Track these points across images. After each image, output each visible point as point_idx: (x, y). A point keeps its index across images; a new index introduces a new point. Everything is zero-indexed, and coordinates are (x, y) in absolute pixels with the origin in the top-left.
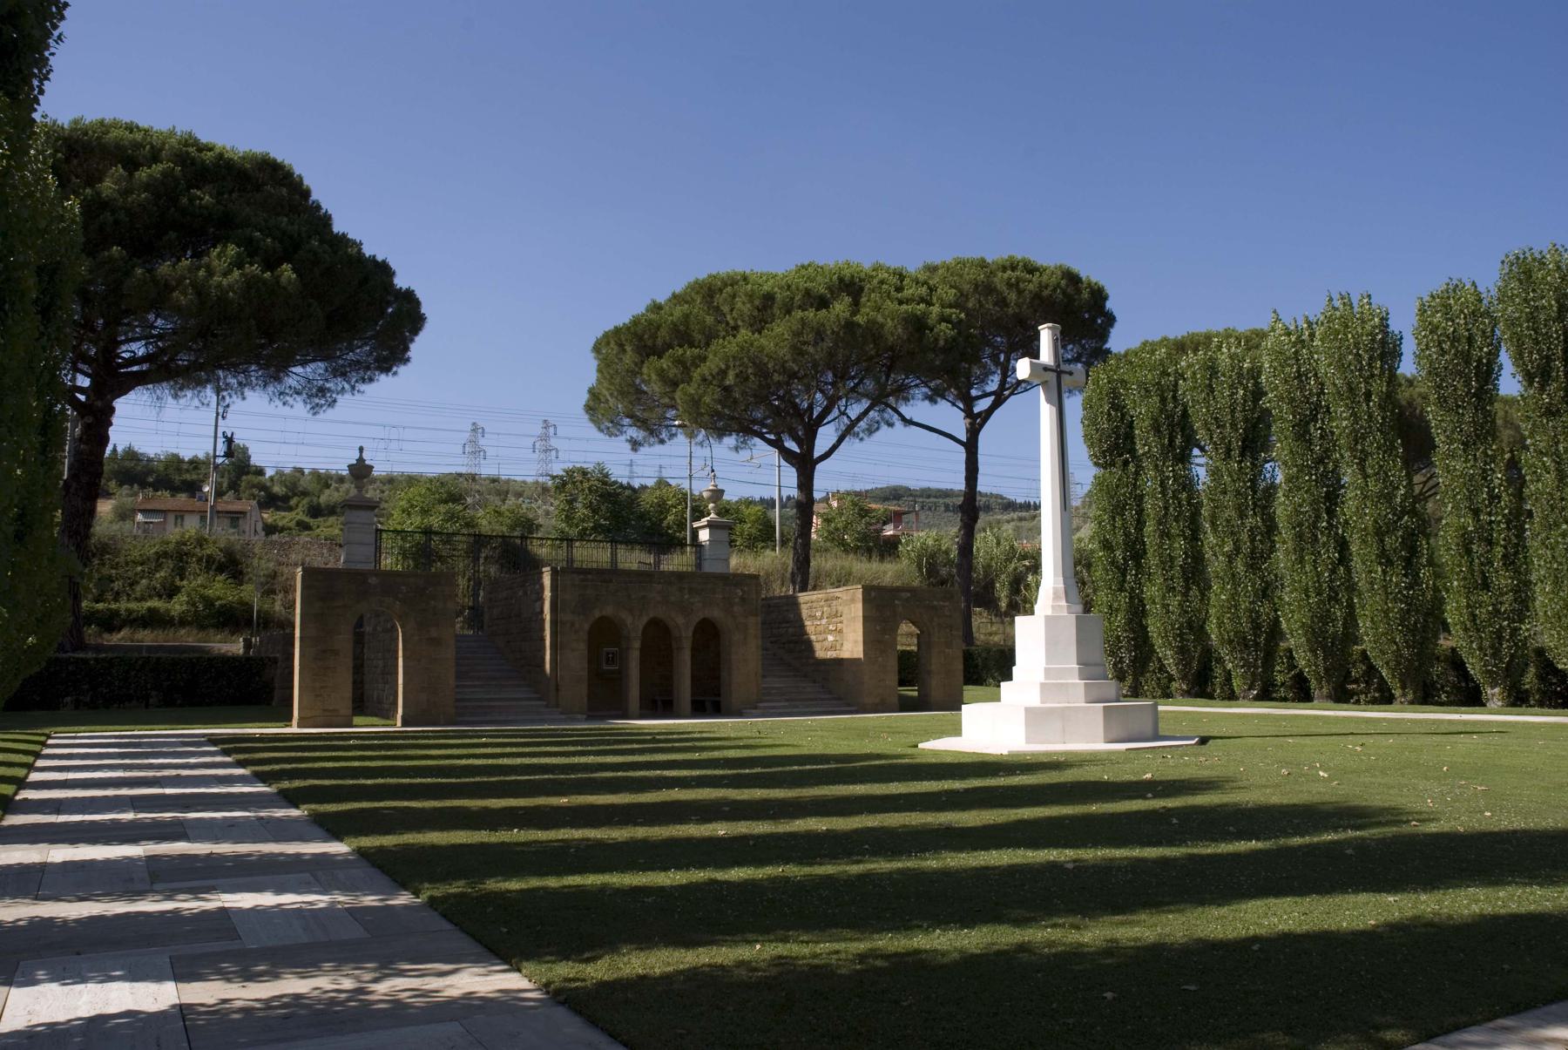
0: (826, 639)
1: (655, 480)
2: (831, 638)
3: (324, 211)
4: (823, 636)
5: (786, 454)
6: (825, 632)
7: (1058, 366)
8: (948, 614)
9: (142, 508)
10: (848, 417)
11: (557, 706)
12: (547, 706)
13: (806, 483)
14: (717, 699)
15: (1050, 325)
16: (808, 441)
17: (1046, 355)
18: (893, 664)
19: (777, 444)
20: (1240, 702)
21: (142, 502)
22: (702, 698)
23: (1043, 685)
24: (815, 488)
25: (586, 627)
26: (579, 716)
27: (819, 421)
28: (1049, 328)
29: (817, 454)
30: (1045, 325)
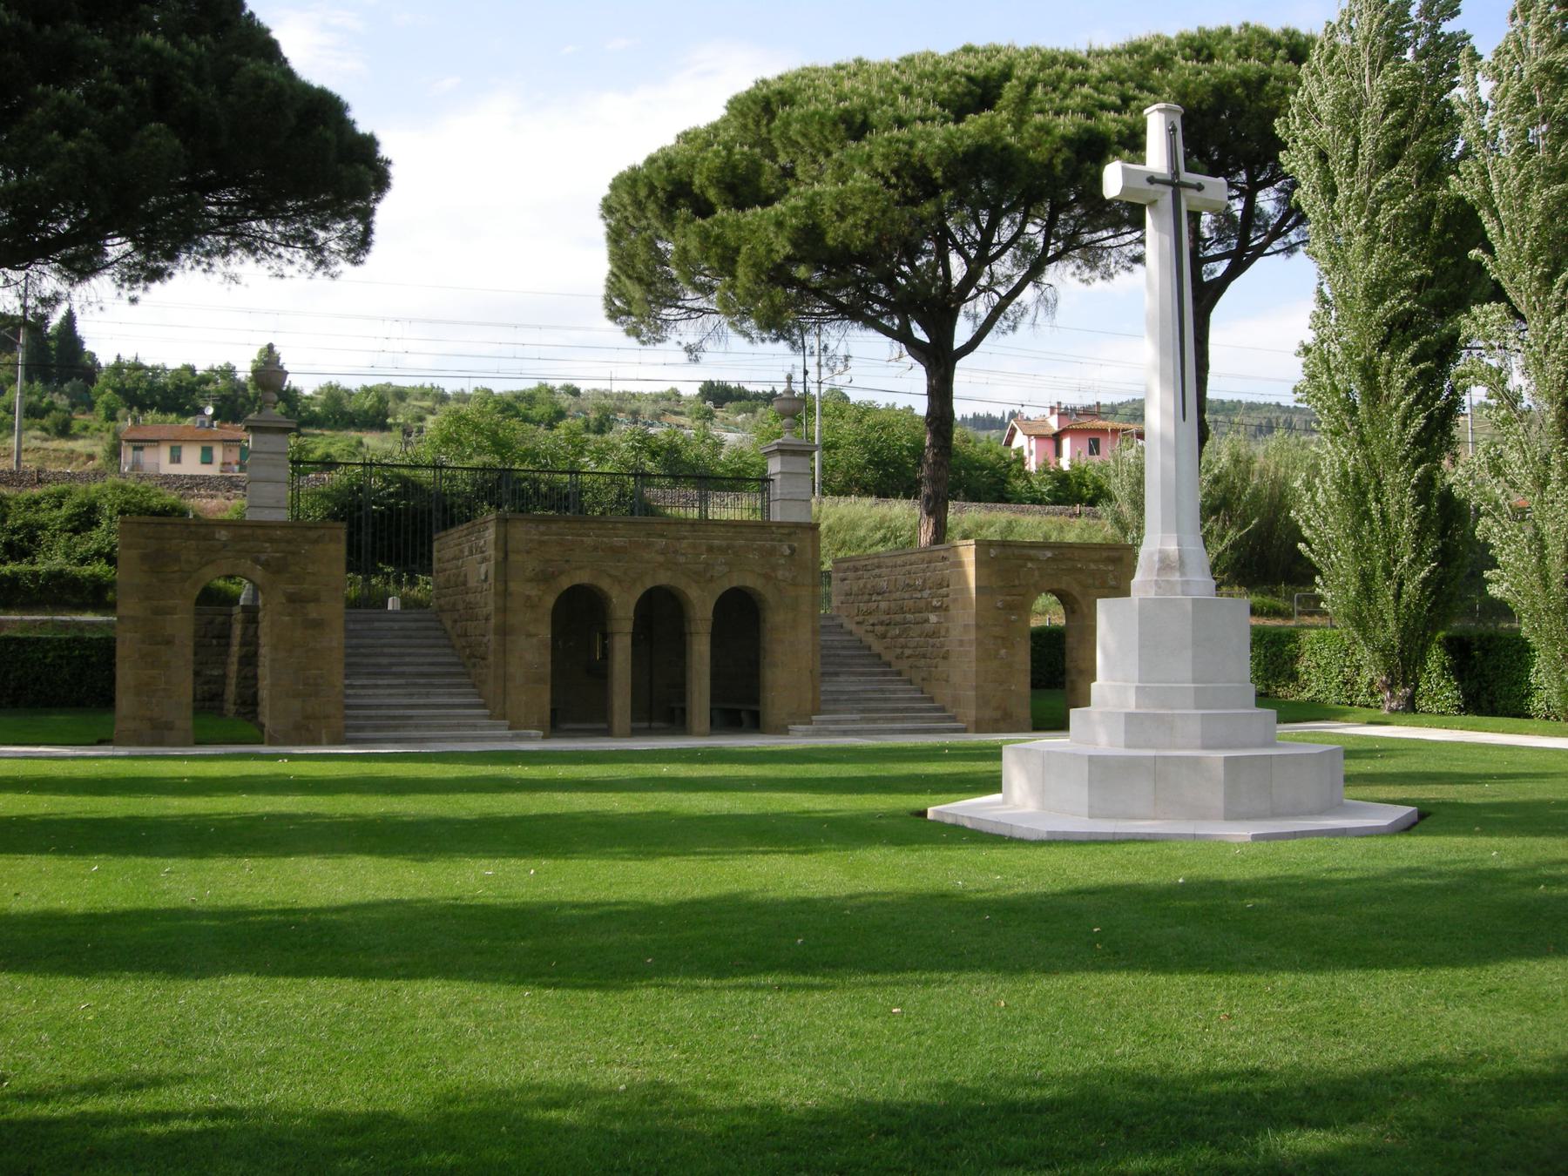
0: (927, 621)
1: (700, 385)
2: (933, 618)
3: (247, 11)
4: (924, 615)
5: (915, 347)
6: (927, 610)
7: (1176, 173)
8: (1113, 583)
9: (129, 437)
10: (997, 293)
11: (504, 717)
12: (490, 717)
13: (941, 391)
14: (753, 708)
15: (1162, 105)
16: (942, 324)
17: (1157, 156)
18: (1022, 657)
19: (904, 336)
20: (1425, 718)
21: (131, 429)
22: (737, 707)
23: (1137, 687)
24: (955, 394)
25: (550, 601)
26: (533, 732)
27: (961, 294)
28: (1160, 110)
29: (957, 344)
30: (1154, 107)
